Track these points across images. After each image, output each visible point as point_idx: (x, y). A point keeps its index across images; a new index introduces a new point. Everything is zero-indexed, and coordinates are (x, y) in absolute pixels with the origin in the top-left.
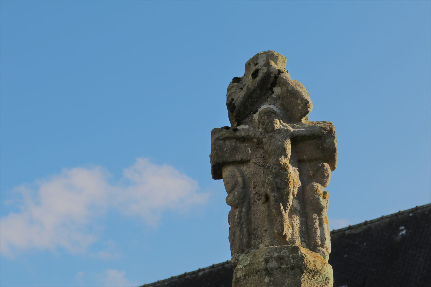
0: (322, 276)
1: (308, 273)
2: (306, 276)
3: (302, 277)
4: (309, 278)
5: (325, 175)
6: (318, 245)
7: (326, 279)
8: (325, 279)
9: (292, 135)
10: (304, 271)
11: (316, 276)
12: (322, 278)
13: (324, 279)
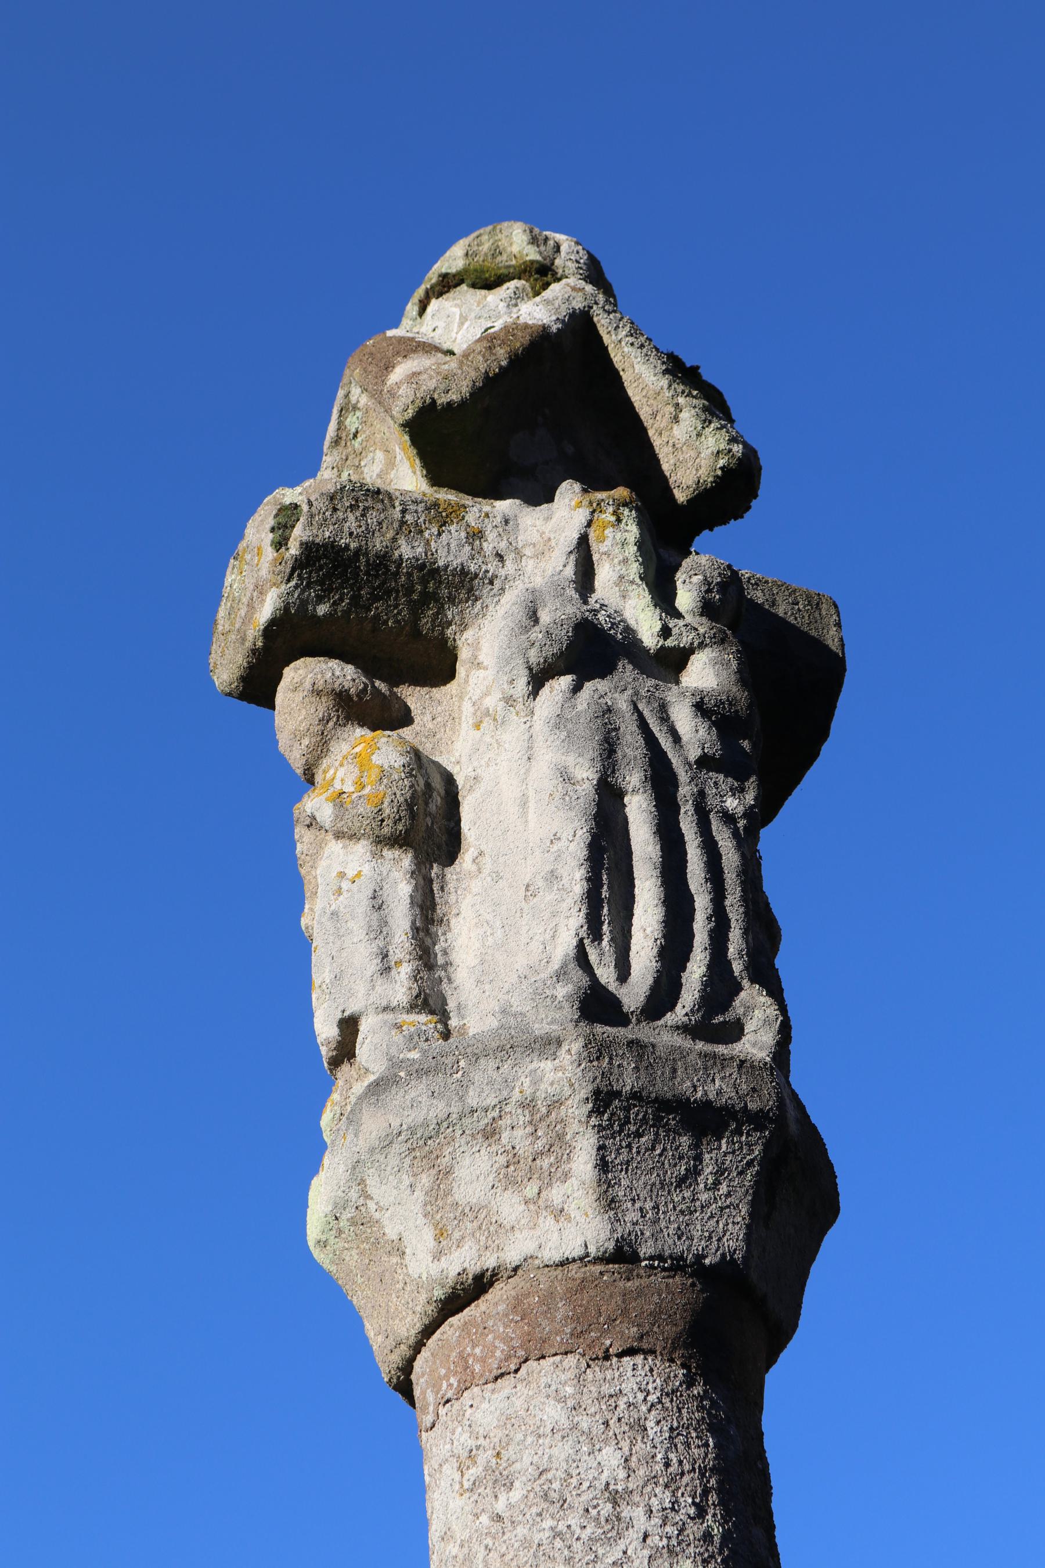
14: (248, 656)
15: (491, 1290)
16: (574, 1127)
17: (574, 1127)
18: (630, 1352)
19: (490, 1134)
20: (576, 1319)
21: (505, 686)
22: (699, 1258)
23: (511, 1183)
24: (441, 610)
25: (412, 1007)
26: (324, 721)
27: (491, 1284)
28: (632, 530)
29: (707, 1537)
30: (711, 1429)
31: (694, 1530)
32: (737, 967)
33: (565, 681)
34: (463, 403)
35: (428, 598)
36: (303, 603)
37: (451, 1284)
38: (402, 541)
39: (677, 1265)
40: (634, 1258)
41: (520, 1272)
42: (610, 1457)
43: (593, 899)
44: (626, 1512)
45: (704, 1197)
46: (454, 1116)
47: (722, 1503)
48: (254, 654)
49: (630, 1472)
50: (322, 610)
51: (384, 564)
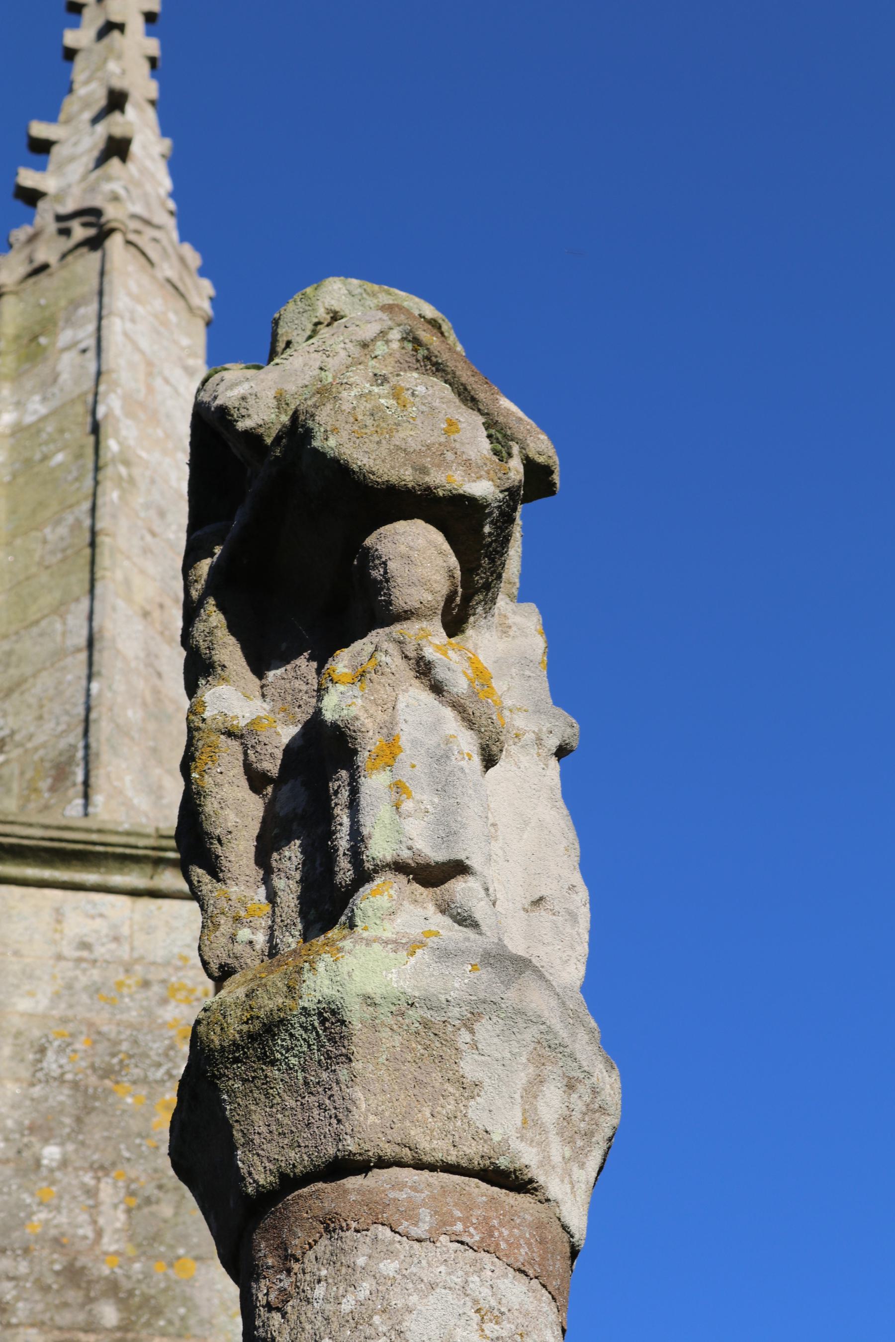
0: (297, 1025)
1: (235, 1066)
2: (238, 1085)
3: (224, 1100)
4: (254, 1078)
5: (375, 579)
6: (347, 890)
7: (323, 1021)
8: (316, 1024)
9: (295, 416)
10: (214, 1075)
11: (274, 1045)
12: (305, 1029)
13: (314, 1028)
14: (420, 485)
15: (522, 1195)
21: (544, 729)
27: (527, 1191)
37: (517, 1166)
41: (546, 1204)
46: (568, 1050)
48: (425, 490)
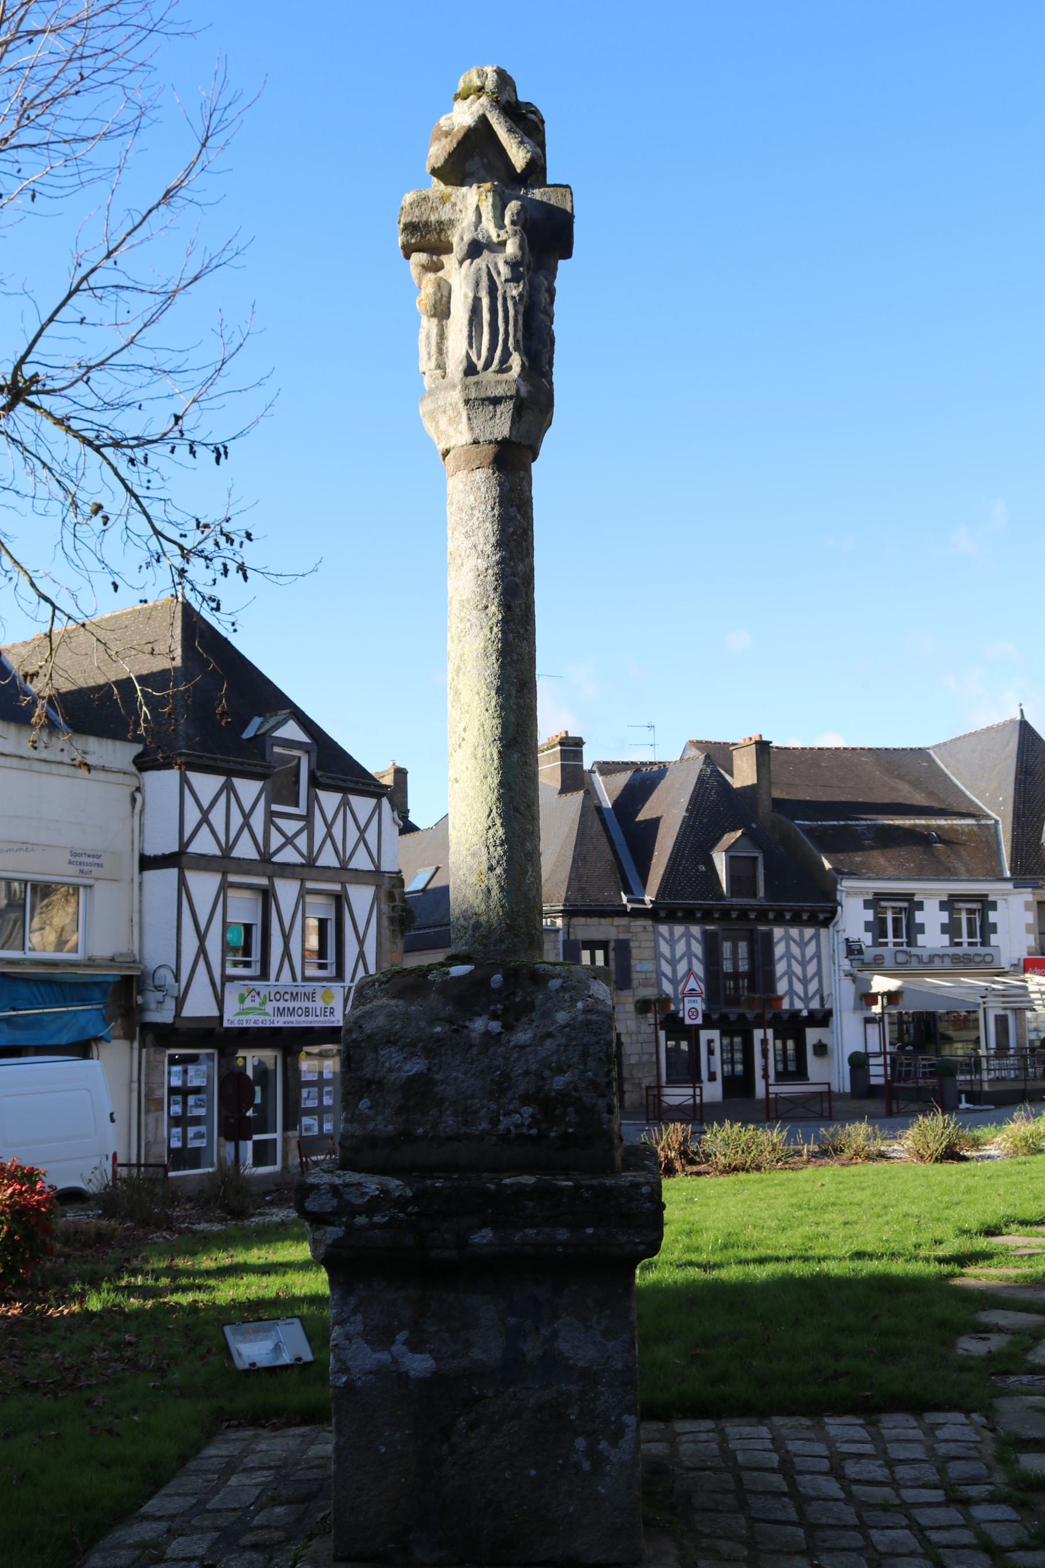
16: (461, 410)
17: (461, 410)
18: (478, 468)
19: (445, 412)
20: (466, 461)
22: (496, 439)
23: (451, 424)
24: (446, 233)
25: (436, 369)
26: (420, 274)
28: (490, 200)
29: (494, 516)
30: (499, 485)
31: (491, 514)
32: (511, 348)
33: (468, 261)
34: (442, 166)
35: (441, 230)
36: (408, 241)
38: (432, 215)
39: (490, 442)
40: (479, 443)
42: (472, 498)
43: (470, 337)
44: (474, 512)
45: (497, 421)
47: (499, 505)
49: (476, 500)
50: (413, 241)
51: (427, 224)
